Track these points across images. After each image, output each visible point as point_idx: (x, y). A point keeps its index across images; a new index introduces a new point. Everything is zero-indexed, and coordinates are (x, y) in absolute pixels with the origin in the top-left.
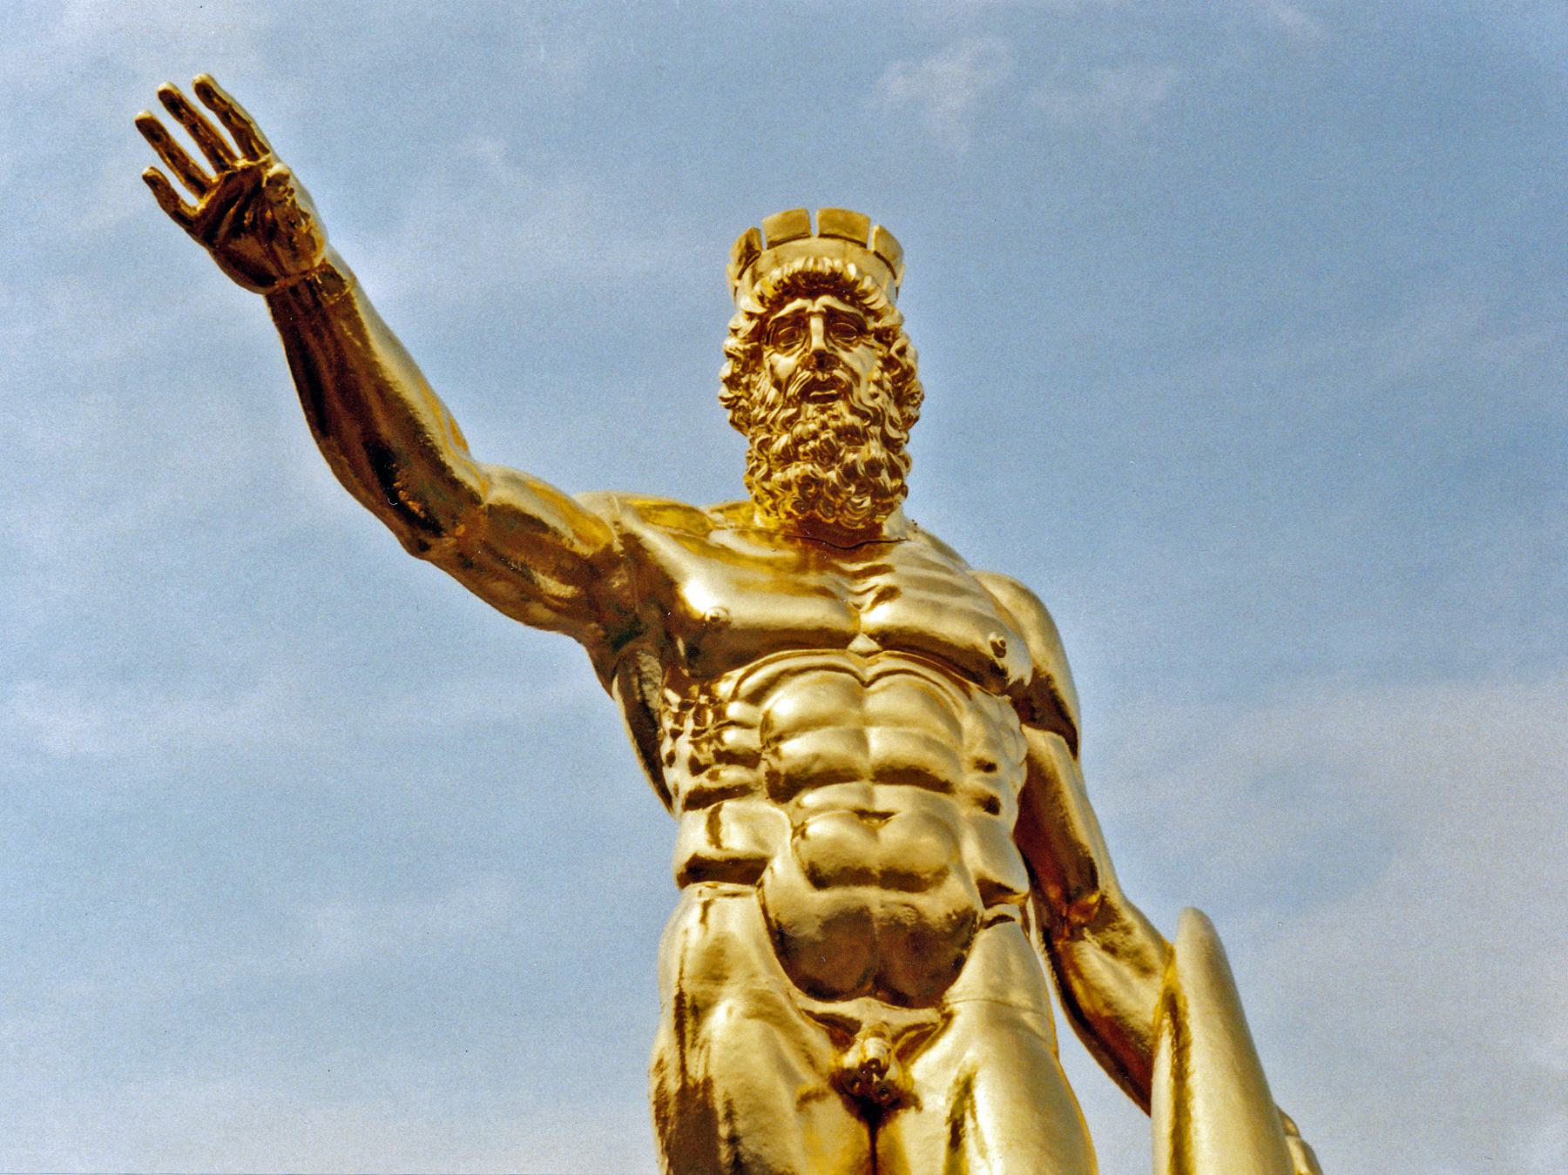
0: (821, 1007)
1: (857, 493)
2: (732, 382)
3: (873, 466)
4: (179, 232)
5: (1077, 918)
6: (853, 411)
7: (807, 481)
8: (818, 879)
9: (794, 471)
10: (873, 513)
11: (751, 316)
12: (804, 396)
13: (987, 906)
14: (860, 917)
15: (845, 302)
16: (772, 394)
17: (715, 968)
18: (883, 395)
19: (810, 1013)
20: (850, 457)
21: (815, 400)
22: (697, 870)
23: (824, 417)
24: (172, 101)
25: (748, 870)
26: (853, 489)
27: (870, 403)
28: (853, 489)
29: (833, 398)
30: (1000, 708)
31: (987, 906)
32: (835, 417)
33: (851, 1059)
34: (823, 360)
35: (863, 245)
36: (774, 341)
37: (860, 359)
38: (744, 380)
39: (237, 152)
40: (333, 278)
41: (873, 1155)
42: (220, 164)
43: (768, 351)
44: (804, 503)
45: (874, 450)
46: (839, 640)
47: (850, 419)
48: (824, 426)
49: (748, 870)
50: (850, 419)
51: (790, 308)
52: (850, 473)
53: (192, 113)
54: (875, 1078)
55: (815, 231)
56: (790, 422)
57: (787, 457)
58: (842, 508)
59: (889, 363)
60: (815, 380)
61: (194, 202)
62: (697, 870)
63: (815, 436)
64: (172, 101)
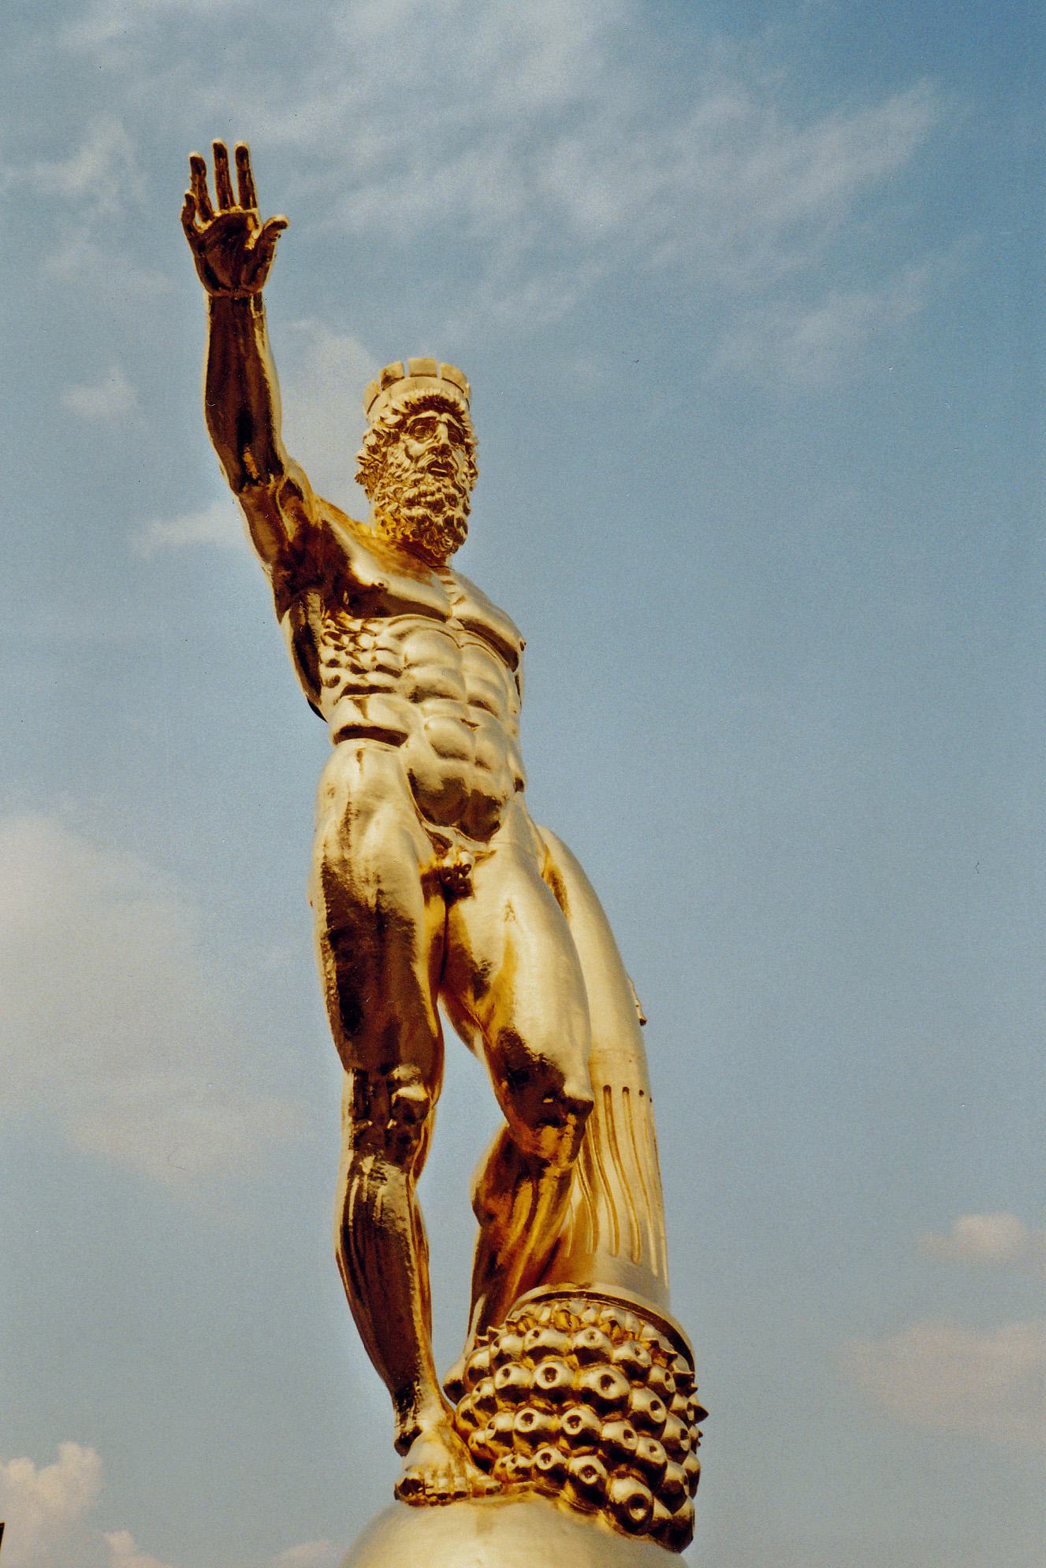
0: (433, 828)
2: (373, 450)
6: (455, 486)
7: (425, 518)
9: (418, 511)
11: (396, 412)
12: (429, 469)
17: (378, 792)
20: (450, 513)
22: (350, 732)
25: (394, 738)
29: (443, 475)
33: (448, 862)
34: (443, 451)
36: (411, 431)
38: (384, 450)
41: (447, 921)
42: (225, 202)
43: (403, 436)
44: (420, 533)
46: (443, 618)
47: (452, 491)
48: (439, 490)
49: (394, 738)
50: (452, 491)
51: (424, 415)
55: (440, 376)
56: (416, 483)
57: (411, 503)
62: (350, 732)
63: (433, 494)
64: (220, 151)
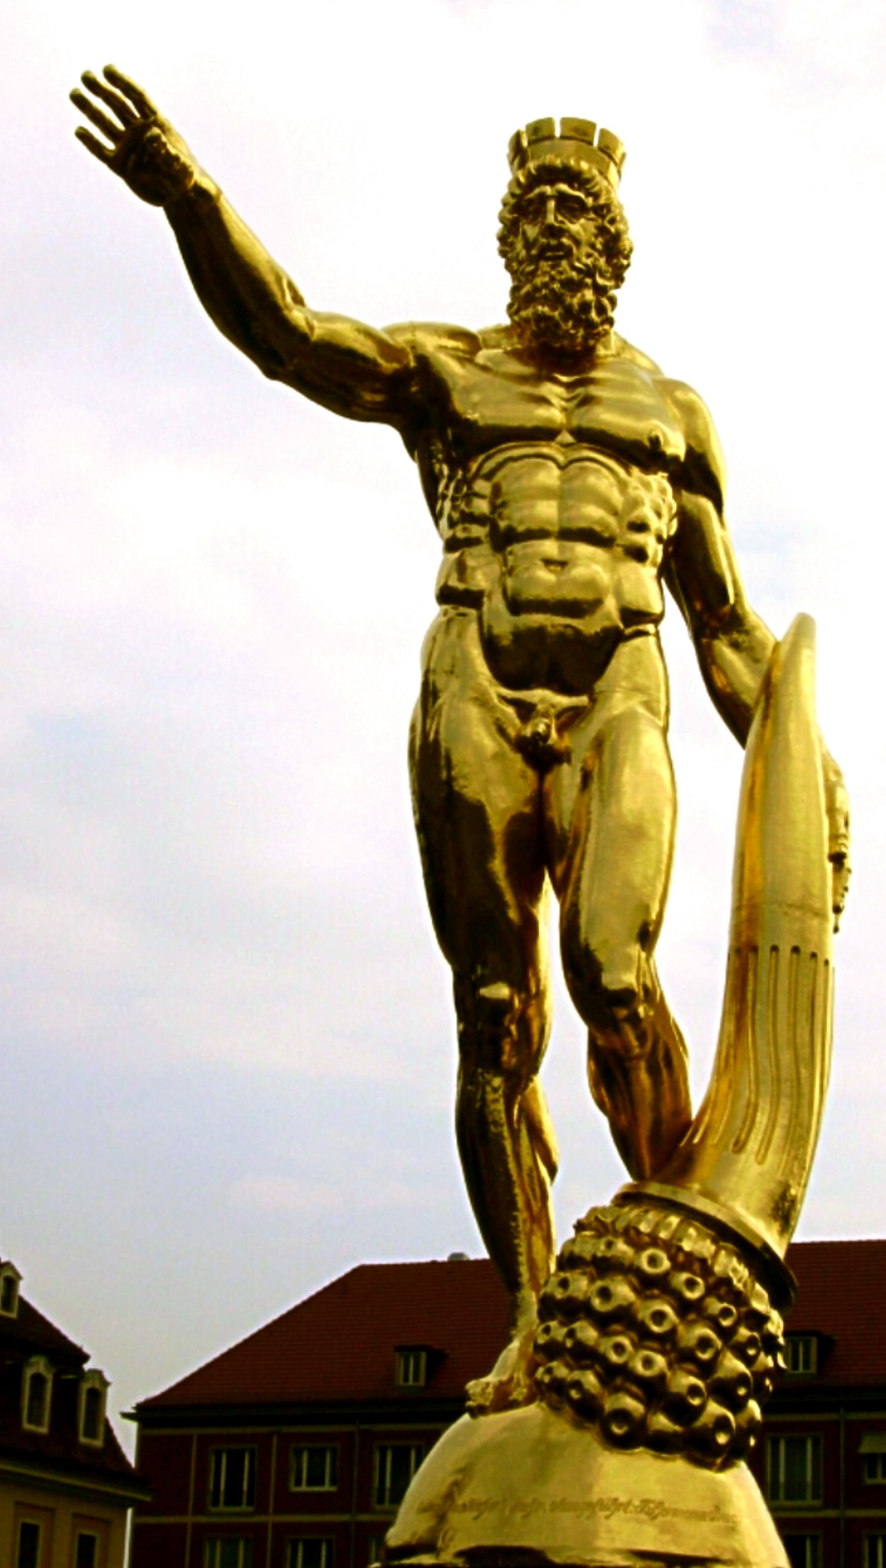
1: (574, 327)
3: (585, 307)
4: (103, 168)
5: (713, 623)
6: (573, 268)
8: (516, 606)
10: (585, 338)
13: (627, 625)
14: (540, 632)
16: (523, 253)
18: (596, 254)
21: (547, 259)
23: (553, 273)
24: (89, 82)
26: (570, 324)
28: (570, 324)
29: (561, 258)
30: (659, 479)
31: (627, 625)
32: (561, 273)
40: (202, 193)
50: (574, 274)
52: (568, 312)
54: (541, 744)
59: (602, 231)
60: (548, 244)
61: (109, 145)
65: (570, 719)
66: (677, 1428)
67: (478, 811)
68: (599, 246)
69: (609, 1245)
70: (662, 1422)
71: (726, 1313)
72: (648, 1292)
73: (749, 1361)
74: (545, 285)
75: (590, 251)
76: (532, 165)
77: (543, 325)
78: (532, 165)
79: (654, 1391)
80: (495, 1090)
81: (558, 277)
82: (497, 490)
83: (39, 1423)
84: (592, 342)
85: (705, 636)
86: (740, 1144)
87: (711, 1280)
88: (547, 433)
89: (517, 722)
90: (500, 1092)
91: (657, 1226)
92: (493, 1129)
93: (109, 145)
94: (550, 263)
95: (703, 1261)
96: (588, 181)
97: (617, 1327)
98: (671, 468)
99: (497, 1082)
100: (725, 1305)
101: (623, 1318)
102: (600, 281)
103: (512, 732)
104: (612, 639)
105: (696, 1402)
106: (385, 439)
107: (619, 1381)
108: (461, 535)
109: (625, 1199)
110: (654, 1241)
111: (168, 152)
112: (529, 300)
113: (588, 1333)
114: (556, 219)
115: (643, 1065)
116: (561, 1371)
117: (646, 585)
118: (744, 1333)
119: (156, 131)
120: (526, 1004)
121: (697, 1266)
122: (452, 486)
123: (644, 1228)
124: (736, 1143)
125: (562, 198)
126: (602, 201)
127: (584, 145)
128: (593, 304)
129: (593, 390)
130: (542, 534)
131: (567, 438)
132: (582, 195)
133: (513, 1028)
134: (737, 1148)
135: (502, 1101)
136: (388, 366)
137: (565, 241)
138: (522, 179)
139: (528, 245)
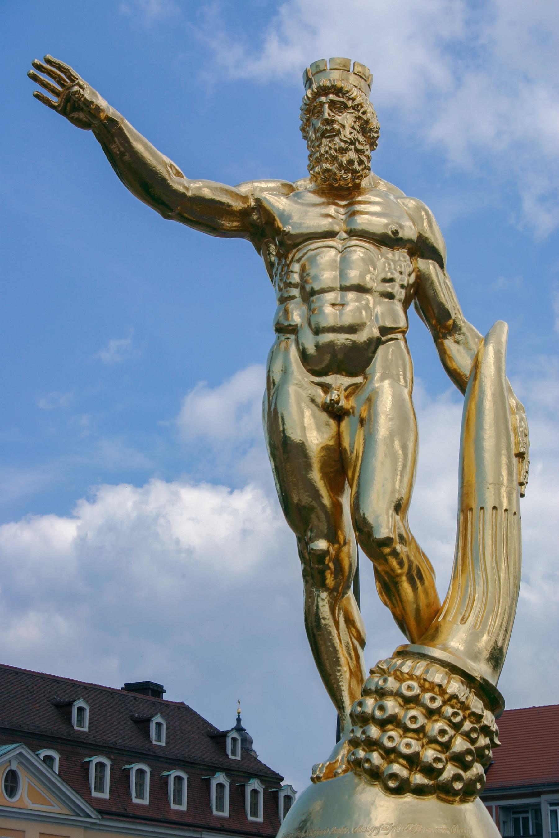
1: (345, 173)
3: (351, 162)
6: (342, 141)
8: (317, 331)
10: (353, 179)
14: (331, 345)
15: (339, 97)
18: (355, 132)
19: (313, 382)
21: (328, 137)
23: (330, 145)
24: (39, 67)
26: (343, 172)
27: (349, 136)
29: (335, 136)
32: (335, 144)
35: (348, 71)
37: (347, 119)
39: (68, 81)
42: (62, 85)
45: (352, 155)
50: (342, 145)
53: (47, 69)
54: (336, 406)
58: (340, 180)
59: (358, 118)
60: (326, 129)
65: (354, 389)
66: (431, 782)
67: (302, 448)
68: (357, 128)
69: (385, 681)
70: (419, 779)
71: (455, 714)
72: (408, 706)
73: (473, 741)
74: (327, 152)
75: (352, 130)
76: (315, 86)
77: (326, 175)
78: (315, 86)
79: (413, 761)
80: (323, 600)
81: (332, 147)
82: (303, 269)
83: (180, 804)
84: (357, 181)
85: (439, 338)
86: (465, 620)
87: (447, 697)
88: (331, 234)
89: (322, 394)
90: (326, 601)
91: (413, 668)
92: (323, 621)
93: (55, 100)
94: (328, 139)
95: (440, 686)
96: (348, 92)
97: (390, 726)
98: (408, 246)
99: (324, 595)
100: (455, 710)
101: (393, 720)
102: (359, 147)
103: (319, 401)
104: (374, 344)
105: (440, 766)
106: (244, 246)
107: (392, 757)
108: (286, 295)
109: (402, 653)
110: (411, 677)
111: (85, 99)
112: (318, 161)
113: (374, 732)
114: (329, 115)
115: (404, 578)
116: (361, 754)
117: (395, 314)
118: (467, 726)
119: (76, 88)
120: (339, 551)
121: (437, 689)
122: (280, 267)
123: (405, 669)
124: (462, 619)
125: (332, 104)
126: (356, 102)
127: (345, 72)
128: (355, 160)
129: (358, 208)
130: (330, 290)
131: (345, 235)
132: (344, 100)
133: (331, 565)
134: (463, 622)
135: (327, 606)
136: (238, 205)
137: (336, 126)
138: (310, 96)
139: (316, 131)
